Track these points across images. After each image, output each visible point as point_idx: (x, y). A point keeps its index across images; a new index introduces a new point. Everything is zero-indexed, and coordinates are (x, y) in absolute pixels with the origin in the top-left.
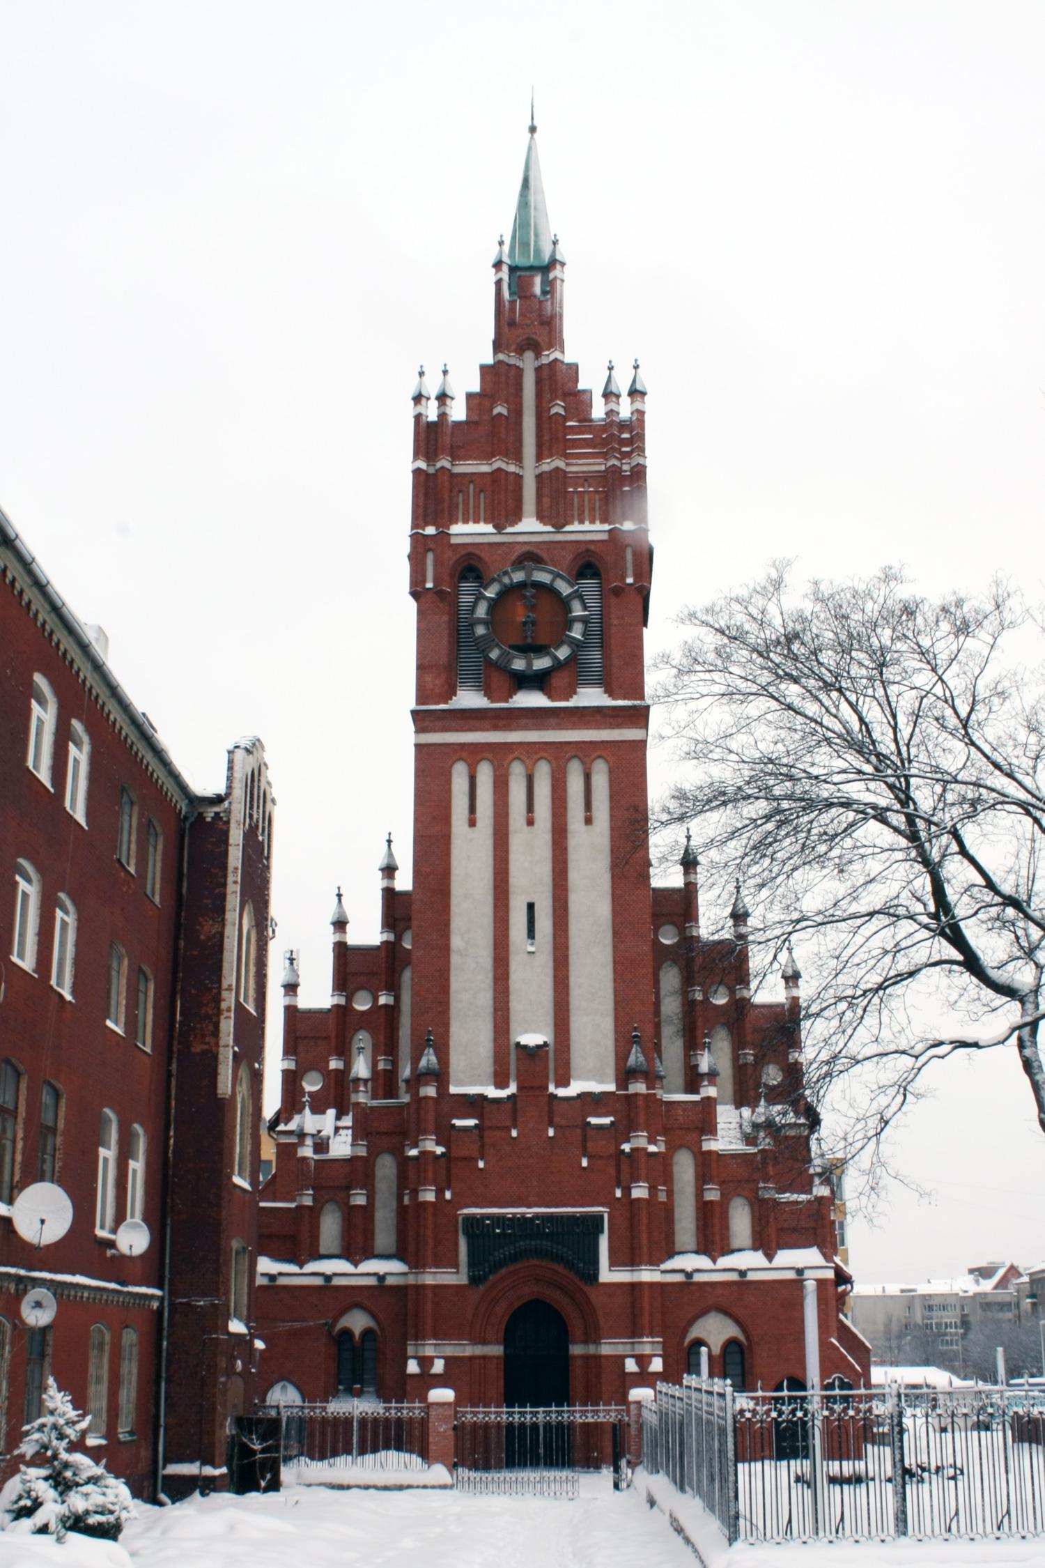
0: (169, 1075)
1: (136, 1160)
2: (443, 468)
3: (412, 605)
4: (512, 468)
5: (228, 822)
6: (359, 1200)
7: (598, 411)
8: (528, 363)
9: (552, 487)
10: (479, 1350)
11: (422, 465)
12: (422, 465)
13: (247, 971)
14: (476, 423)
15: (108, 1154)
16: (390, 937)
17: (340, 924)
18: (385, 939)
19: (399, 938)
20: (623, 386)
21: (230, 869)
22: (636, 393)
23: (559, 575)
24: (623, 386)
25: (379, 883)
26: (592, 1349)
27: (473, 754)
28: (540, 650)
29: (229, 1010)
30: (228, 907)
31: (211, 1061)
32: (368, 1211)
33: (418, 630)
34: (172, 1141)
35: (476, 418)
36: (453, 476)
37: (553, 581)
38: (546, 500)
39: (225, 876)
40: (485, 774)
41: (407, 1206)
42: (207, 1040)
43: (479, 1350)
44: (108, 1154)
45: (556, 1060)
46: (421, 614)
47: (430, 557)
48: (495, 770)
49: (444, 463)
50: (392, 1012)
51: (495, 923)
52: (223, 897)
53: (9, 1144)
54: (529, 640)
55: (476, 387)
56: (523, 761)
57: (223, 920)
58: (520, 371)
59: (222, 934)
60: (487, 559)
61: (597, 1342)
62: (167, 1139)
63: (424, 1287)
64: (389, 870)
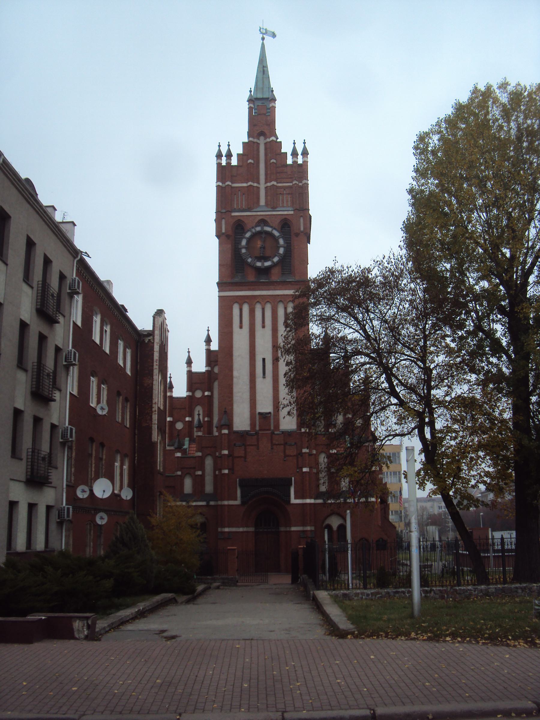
0: (135, 434)
1: (125, 466)
2: (228, 185)
3: (217, 241)
4: (255, 185)
5: (153, 343)
6: (200, 473)
7: (290, 161)
8: (262, 141)
9: (272, 192)
10: (245, 529)
11: (220, 184)
12: (220, 184)
13: (160, 395)
14: (241, 166)
15: (117, 464)
16: (209, 368)
17: (189, 362)
18: (207, 369)
19: (212, 368)
20: (300, 151)
21: (155, 360)
22: (305, 153)
23: (275, 229)
24: (300, 151)
25: (204, 347)
26: (288, 529)
27: (241, 300)
28: (266, 259)
29: (155, 411)
30: (154, 374)
31: (149, 429)
32: (203, 477)
33: (219, 250)
34: (136, 458)
35: (241, 164)
36: (232, 187)
37: (272, 230)
38: (269, 198)
39: (153, 363)
40: (246, 308)
41: (217, 475)
42: (148, 422)
43: (245, 529)
44: (117, 464)
45: (274, 419)
46: (220, 244)
47: (223, 222)
48: (250, 307)
49: (228, 183)
50: (210, 398)
51: (250, 366)
52: (152, 370)
53: (90, 465)
54: (262, 255)
55: (241, 151)
56: (260, 303)
57: (153, 378)
58: (258, 144)
59: (152, 384)
60: (245, 222)
61: (290, 527)
62: (135, 457)
63: (224, 505)
64: (208, 341)
